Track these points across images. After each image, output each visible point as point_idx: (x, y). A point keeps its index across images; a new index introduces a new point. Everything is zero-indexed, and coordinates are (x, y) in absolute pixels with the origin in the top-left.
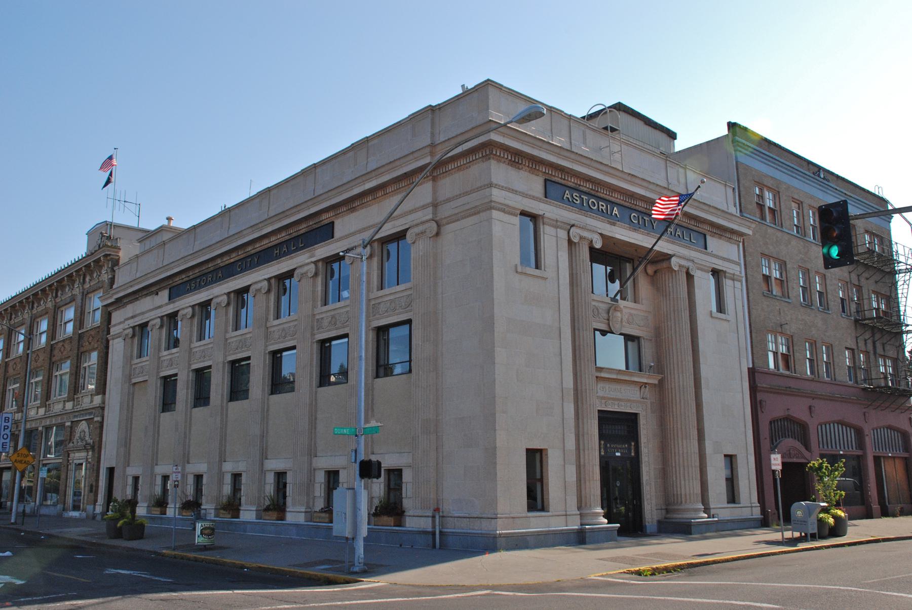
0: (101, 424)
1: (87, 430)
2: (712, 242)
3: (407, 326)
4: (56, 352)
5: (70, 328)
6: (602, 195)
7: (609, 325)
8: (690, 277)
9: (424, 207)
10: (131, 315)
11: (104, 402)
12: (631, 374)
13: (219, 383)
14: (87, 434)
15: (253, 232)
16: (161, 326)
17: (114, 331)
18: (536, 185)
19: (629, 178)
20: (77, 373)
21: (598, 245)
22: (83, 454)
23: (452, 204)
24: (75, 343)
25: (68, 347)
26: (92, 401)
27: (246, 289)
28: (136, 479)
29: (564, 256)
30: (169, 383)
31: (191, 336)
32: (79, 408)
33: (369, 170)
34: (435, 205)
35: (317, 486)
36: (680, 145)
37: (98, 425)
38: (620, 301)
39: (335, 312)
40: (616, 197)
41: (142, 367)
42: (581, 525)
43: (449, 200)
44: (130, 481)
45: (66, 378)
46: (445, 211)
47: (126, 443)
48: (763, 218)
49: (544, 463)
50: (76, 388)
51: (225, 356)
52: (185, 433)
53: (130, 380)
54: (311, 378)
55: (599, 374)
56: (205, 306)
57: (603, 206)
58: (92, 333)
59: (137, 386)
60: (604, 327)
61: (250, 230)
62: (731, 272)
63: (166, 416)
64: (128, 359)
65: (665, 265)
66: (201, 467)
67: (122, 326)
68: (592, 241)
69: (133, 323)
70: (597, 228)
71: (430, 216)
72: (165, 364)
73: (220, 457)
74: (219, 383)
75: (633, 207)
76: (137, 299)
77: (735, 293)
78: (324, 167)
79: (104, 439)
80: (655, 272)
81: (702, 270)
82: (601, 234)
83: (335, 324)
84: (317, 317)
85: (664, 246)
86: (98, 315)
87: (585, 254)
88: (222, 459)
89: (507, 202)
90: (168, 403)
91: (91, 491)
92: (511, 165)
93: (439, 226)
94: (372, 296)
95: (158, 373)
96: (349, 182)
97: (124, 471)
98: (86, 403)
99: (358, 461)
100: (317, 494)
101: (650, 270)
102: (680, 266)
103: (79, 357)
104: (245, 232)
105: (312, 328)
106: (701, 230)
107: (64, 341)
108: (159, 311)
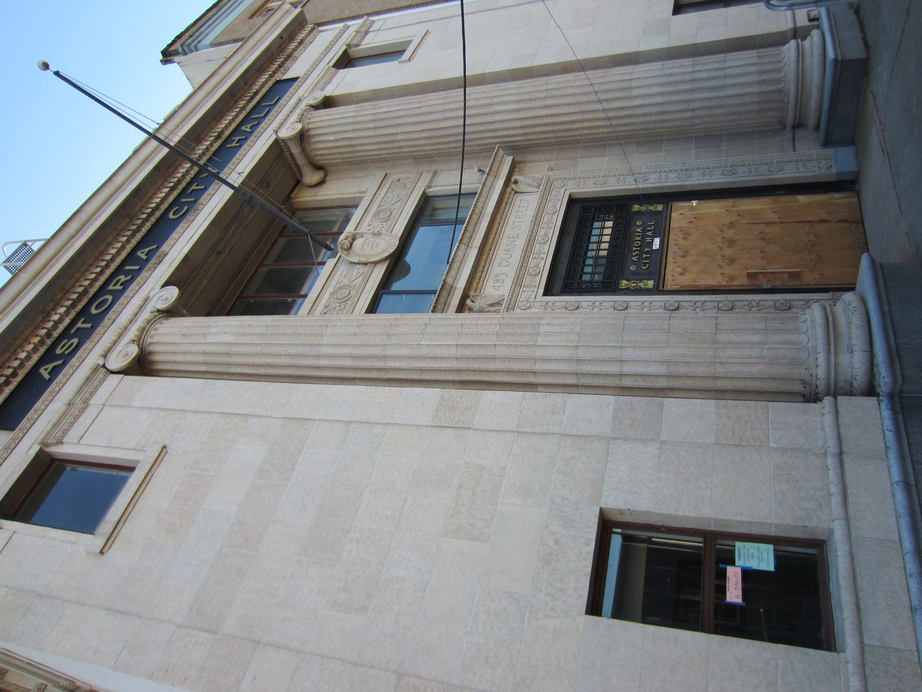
42: (871, 391)
80: (319, 168)
82: (166, 284)
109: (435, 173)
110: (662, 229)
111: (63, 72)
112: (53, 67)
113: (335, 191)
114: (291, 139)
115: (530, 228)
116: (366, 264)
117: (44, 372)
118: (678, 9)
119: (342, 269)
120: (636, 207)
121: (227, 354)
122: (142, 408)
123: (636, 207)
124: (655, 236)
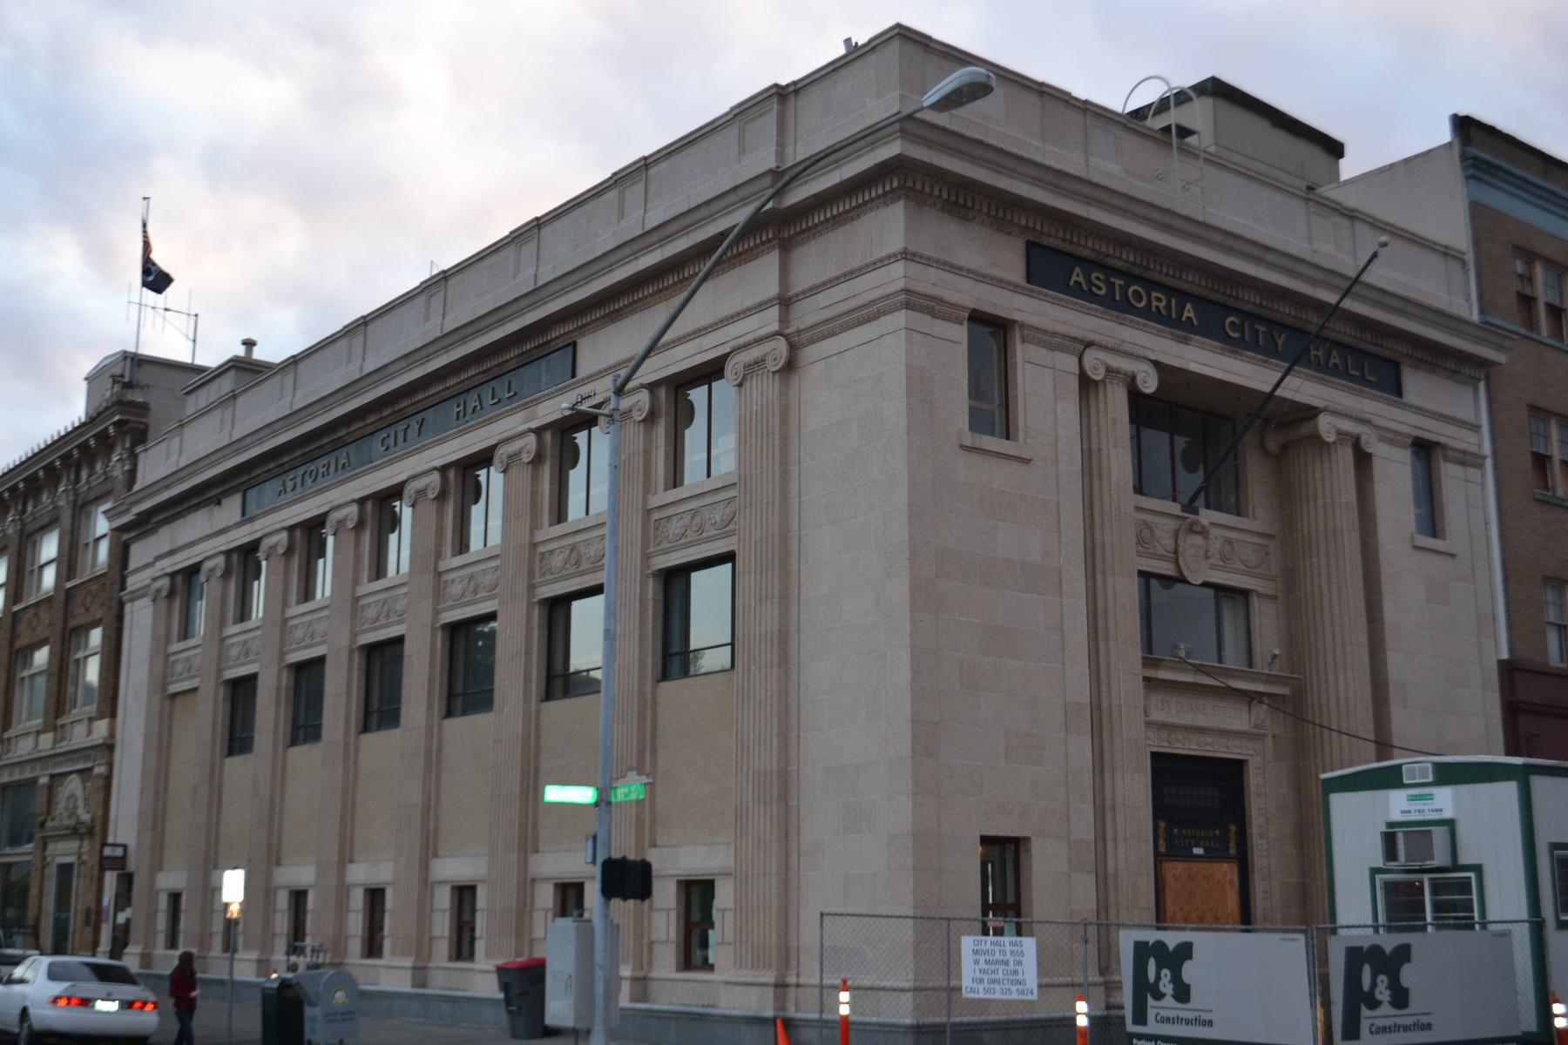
0: (108, 779)
1: (79, 792)
2: (1417, 385)
3: (727, 568)
4: (22, 628)
5: (49, 578)
6: (1157, 277)
7: (1177, 562)
8: (1363, 460)
9: (761, 307)
10: (167, 548)
11: (112, 734)
12: (1230, 673)
13: (340, 692)
14: (80, 803)
15: (409, 368)
16: (227, 573)
17: (133, 582)
18: (1009, 260)
19: (1123, 204)
20: (64, 671)
21: (1149, 383)
22: (73, 845)
23: (822, 299)
24: (58, 606)
25: (45, 617)
26: (89, 733)
27: (396, 492)
28: (175, 898)
29: (1069, 408)
30: (241, 691)
31: (286, 592)
32: (64, 747)
33: (647, 228)
34: (785, 302)
35: (437, 917)
36: (1349, 168)
37: (101, 783)
38: (1203, 511)
39: (578, 538)
40: (1190, 282)
41: (188, 659)
42: (1108, 1007)
43: (814, 290)
44: (163, 902)
45: (41, 682)
46: (807, 314)
47: (155, 819)
48: (1531, 324)
49: (1023, 871)
50: (59, 704)
51: (354, 635)
52: (272, 801)
53: (165, 685)
54: (527, 680)
55: (1152, 673)
56: (313, 529)
57: (1159, 301)
58: (93, 587)
59: (178, 700)
60: (1166, 568)
61: (403, 363)
62: (1462, 446)
63: (236, 764)
64: (161, 642)
65: (1305, 430)
66: (299, 873)
67: (149, 573)
68: (1134, 378)
69: (170, 565)
70: (1146, 349)
71: (775, 327)
72: (234, 652)
73: (342, 851)
74: (340, 692)
75: (1231, 302)
76: (179, 515)
77: (1473, 498)
78: (557, 225)
79: (112, 814)
80: (1285, 447)
81: (1392, 442)
82: (1157, 364)
83: (578, 563)
84: (542, 549)
85: (1301, 388)
86: (103, 550)
87: (1116, 404)
88: (346, 856)
89: (937, 292)
90: (238, 739)
91: (87, 923)
92: (950, 212)
93: (793, 348)
94: (654, 501)
95: (220, 671)
96: (605, 255)
97: (152, 881)
98: (79, 737)
99: (600, 860)
100: (278, 930)
101: (1273, 444)
102: (1340, 433)
103: (68, 641)
104: (393, 369)
105: (531, 573)
106: (1386, 353)
107: (37, 605)
108: (222, 539)
109: (1275, 598)
110: (1213, 855)
111: (1377, 262)
112: (1382, 251)
113: (1256, 473)
114: (1316, 427)
115: (1216, 728)
116: (1176, 553)
117: (1077, 276)
118: (341, 1042)
119: (1170, 525)
120: (1233, 828)
121: (1100, 477)
122: (1055, 414)
123: (1233, 828)
124: (1205, 849)
